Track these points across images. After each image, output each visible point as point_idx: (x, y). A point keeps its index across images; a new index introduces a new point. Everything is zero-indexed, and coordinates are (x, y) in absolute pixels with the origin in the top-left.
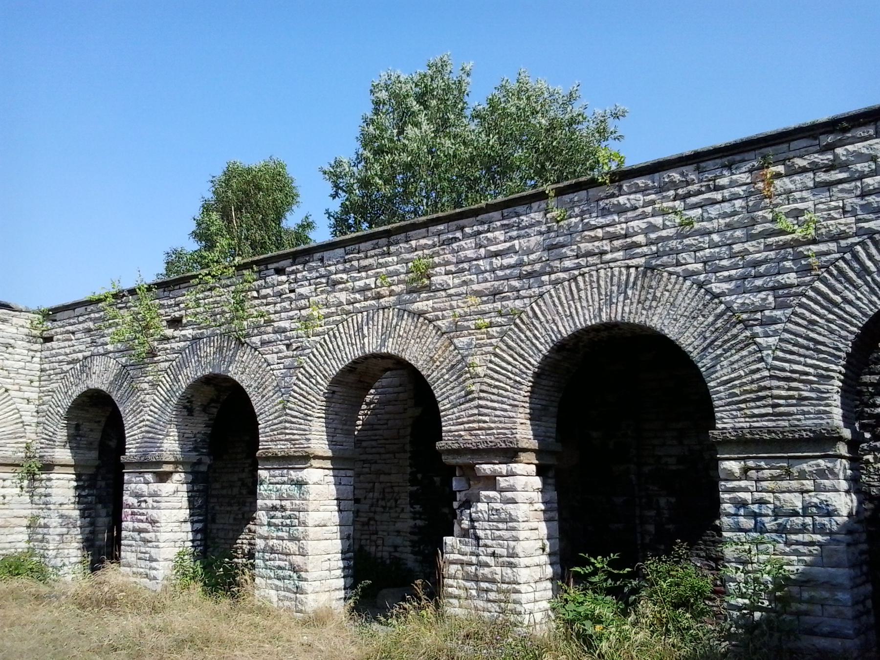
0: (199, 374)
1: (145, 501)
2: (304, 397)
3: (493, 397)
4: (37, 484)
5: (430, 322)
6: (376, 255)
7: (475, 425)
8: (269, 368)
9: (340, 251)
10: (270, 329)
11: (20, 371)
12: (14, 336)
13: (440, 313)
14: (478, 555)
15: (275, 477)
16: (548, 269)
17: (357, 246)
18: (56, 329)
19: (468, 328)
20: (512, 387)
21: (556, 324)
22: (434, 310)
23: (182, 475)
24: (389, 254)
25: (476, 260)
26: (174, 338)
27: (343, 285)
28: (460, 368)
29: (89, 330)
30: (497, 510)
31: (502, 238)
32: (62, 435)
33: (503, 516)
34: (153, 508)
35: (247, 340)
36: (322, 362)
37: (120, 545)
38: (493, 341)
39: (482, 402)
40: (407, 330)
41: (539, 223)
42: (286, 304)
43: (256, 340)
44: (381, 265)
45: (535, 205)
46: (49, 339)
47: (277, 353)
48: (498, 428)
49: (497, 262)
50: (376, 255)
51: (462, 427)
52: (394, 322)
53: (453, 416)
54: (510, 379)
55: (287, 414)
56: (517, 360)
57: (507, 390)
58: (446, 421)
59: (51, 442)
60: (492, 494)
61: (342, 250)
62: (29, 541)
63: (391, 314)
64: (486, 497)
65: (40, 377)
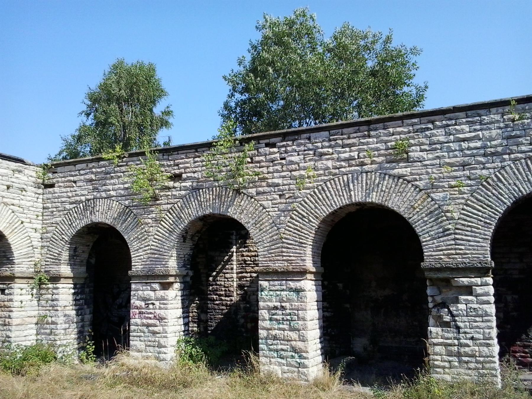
0: (200, 213)
1: (153, 304)
2: (299, 231)
3: (467, 233)
4: (43, 292)
5: (409, 182)
6: (357, 137)
7: (453, 252)
8: (264, 210)
9: (326, 133)
10: (264, 184)
11: (31, 208)
12: (27, 183)
13: (417, 177)
14: (458, 339)
15: (274, 286)
16: (508, 151)
17: (340, 130)
18: (57, 178)
19: (443, 187)
20: (482, 226)
21: (517, 186)
22: (412, 174)
23: (179, 284)
24: (369, 136)
25: (446, 143)
26: (174, 188)
27: (329, 156)
28: (438, 213)
29: (91, 180)
30: (474, 309)
31: (468, 130)
32: (65, 255)
33: (480, 312)
34: (160, 308)
35: (244, 191)
36: (313, 207)
37: (129, 336)
38: (465, 196)
39: (457, 236)
40: (389, 187)
41: (498, 121)
42: (279, 167)
43: (253, 191)
44: (363, 144)
45: (494, 110)
46: (52, 186)
47: (271, 200)
48: (472, 254)
49: (465, 145)
50: (357, 137)
51: (441, 253)
52: (377, 181)
53: (434, 246)
54: (481, 221)
55: (283, 243)
56: (486, 209)
57: (478, 229)
58: (427, 249)
59: (57, 261)
60: (470, 298)
61: (327, 133)
62: (37, 334)
63: (373, 176)
64: (464, 300)
65: (43, 213)
